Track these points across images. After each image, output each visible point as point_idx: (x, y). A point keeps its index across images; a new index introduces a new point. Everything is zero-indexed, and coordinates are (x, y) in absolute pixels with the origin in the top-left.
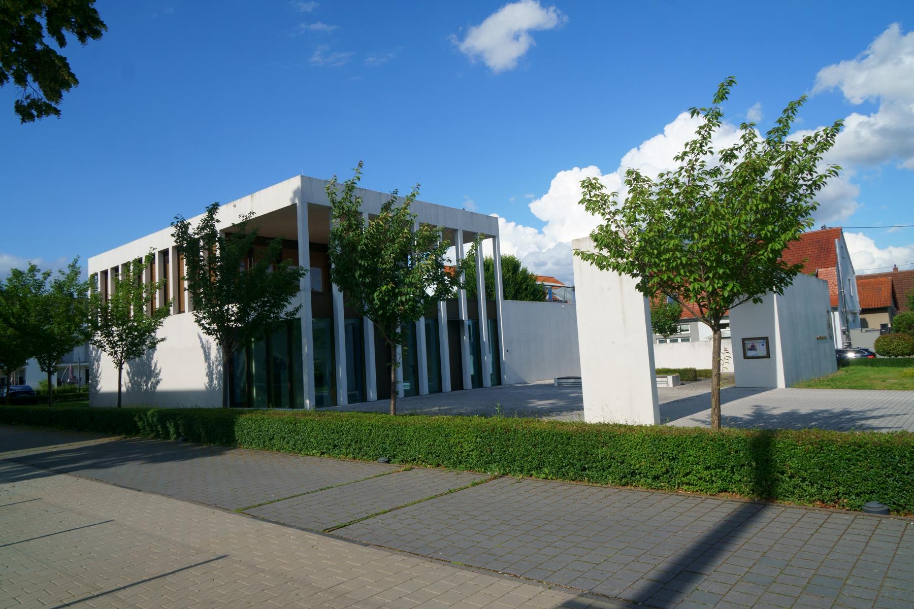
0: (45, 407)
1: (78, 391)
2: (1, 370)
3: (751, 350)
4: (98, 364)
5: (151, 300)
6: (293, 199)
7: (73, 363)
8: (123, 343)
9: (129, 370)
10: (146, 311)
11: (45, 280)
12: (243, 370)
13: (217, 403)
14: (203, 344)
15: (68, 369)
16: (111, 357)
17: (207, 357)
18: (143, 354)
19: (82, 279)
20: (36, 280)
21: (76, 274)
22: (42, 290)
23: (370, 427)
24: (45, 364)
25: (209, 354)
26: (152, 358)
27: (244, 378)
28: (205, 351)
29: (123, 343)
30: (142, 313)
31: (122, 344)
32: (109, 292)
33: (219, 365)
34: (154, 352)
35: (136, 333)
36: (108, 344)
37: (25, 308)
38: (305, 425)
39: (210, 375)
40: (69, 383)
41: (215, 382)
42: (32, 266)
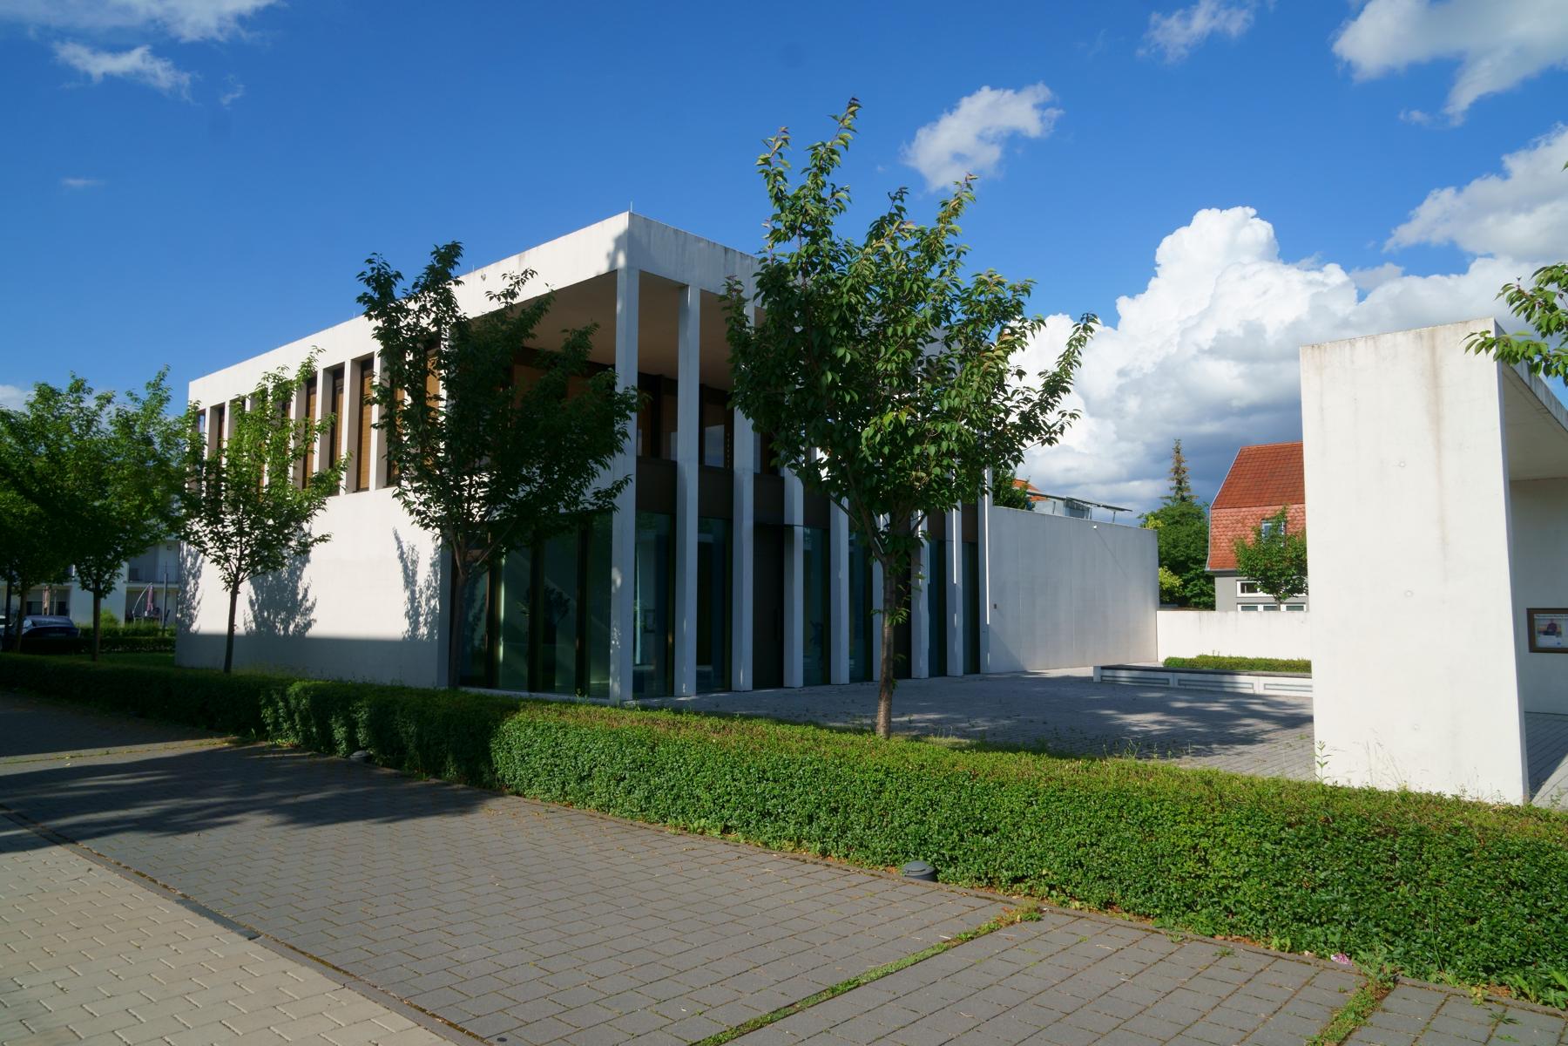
0: (83, 661)
1: (160, 633)
2: (1567, 938)
3: (1546, 633)
4: (197, 583)
5: (304, 455)
6: (613, 258)
7: (157, 582)
8: (244, 540)
9: (254, 597)
10: (294, 478)
11: (101, 409)
12: (481, 610)
13: (429, 675)
14: (402, 553)
15: (147, 592)
16: (215, 567)
17: (410, 580)
18: (283, 565)
19: (171, 414)
20: (82, 409)
21: (161, 402)
22: (94, 429)
23: (881, 776)
24: (89, 575)
25: (415, 573)
26: (299, 577)
27: (482, 629)
28: (405, 568)
29: (244, 540)
30: (285, 481)
31: (240, 541)
32: (226, 436)
33: (432, 597)
34: (304, 565)
35: (271, 522)
36: (211, 539)
37: (58, 462)
38: (681, 753)
39: (413, 615)
40: (145, 618)
41: (423, 630)
42: (77, 381)
